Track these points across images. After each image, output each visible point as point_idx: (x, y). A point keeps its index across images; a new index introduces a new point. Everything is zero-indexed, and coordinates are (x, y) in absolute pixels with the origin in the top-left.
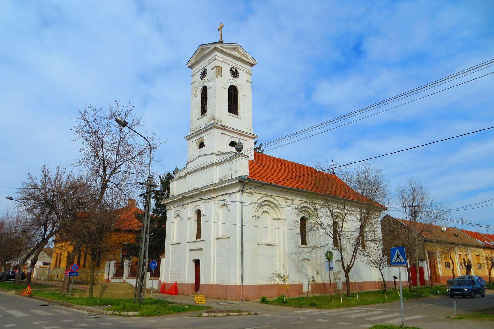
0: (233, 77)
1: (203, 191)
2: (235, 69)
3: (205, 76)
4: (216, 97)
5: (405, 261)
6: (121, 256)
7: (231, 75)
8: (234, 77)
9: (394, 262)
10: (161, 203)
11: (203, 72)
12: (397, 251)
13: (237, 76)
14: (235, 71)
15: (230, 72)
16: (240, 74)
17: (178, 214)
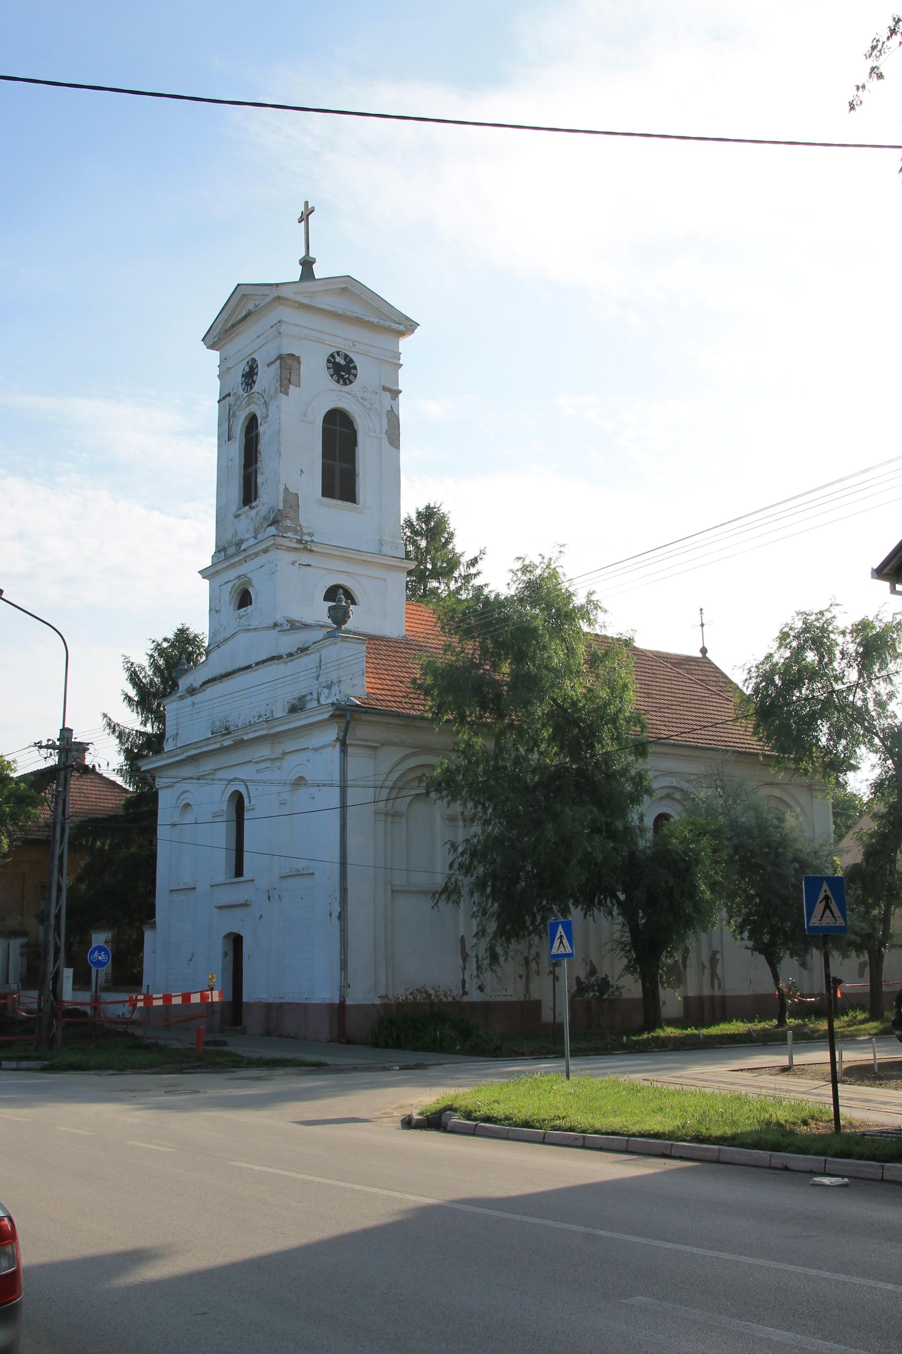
0: (338, 382)
1: (246, 738)
2: (346, 356)
3: (254, 382)
4: (280, 454)
5: (844, 924)
6: (58, 905)
7: (332, 376)
8: (342, 382)
9: (817, 924)
10: (140, 768)
11: (247, 369)
12: (560, 929)
13: (351, 377)
14: (343, 362)
15: (328, 368)
16: (360, 372)
17: (184, 802)
